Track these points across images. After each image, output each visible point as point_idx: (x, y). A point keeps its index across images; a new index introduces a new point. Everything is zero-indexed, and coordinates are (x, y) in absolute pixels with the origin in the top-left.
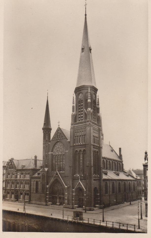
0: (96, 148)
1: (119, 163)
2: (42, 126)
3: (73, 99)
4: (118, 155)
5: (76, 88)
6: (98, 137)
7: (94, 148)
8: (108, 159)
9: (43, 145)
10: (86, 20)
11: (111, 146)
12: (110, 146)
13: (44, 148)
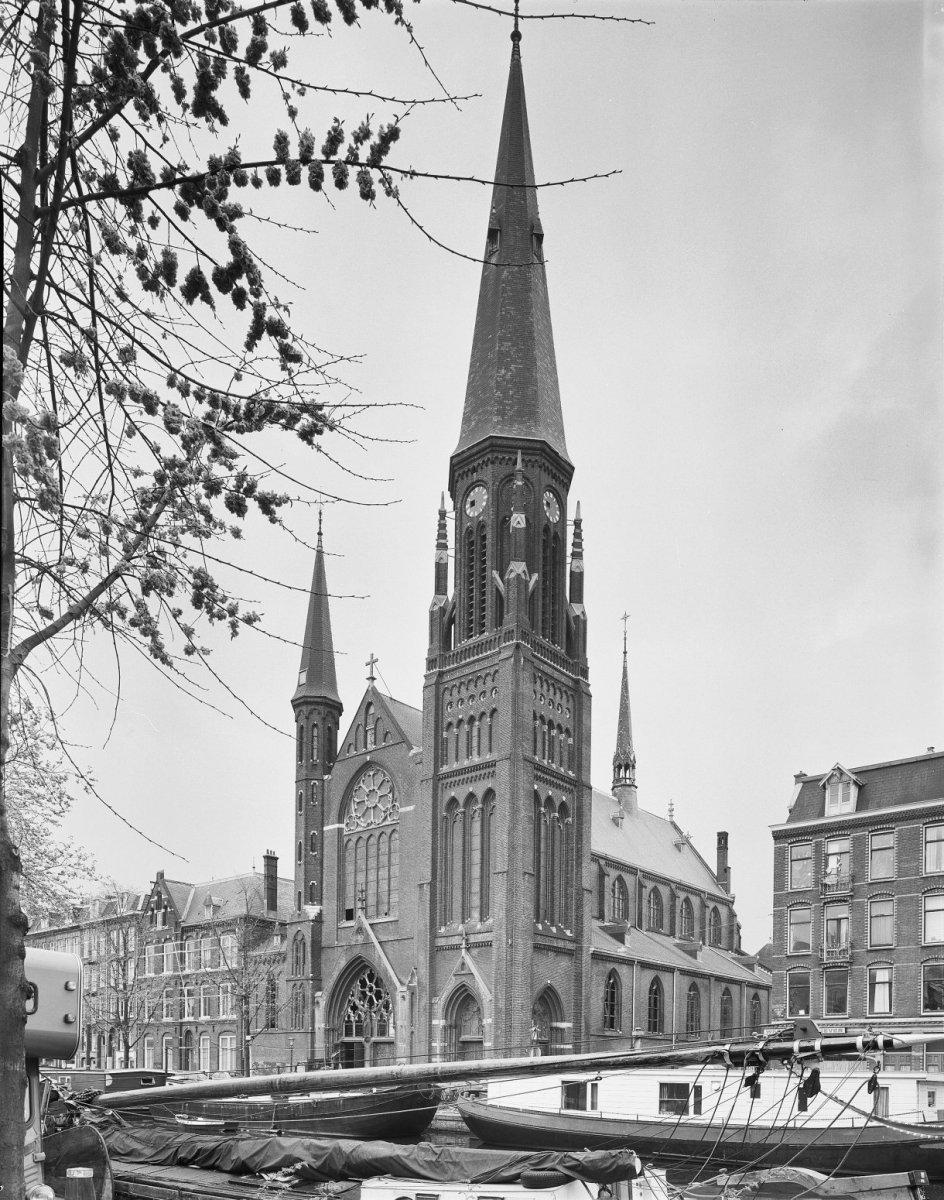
0: (558, 787)
1: (711, 905)
3: (442, 526)
4: (713, 874)
5: (452, 458)
6: (567, 731)
8: (644, 877)
9: (297, 789)
11: (676, 827)
12: (673, 823)
13: (300, 803)
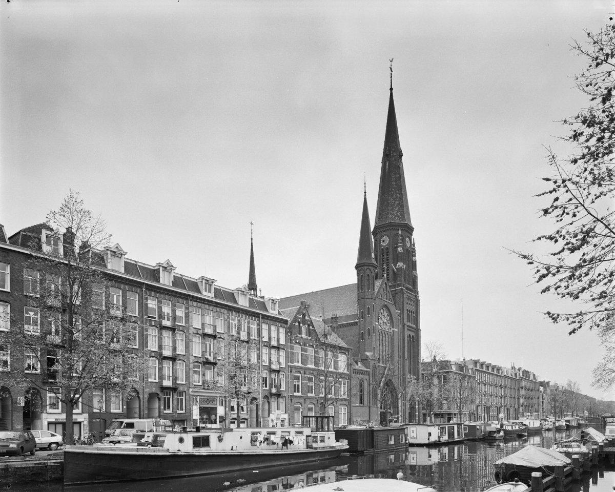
7: (408, 329)
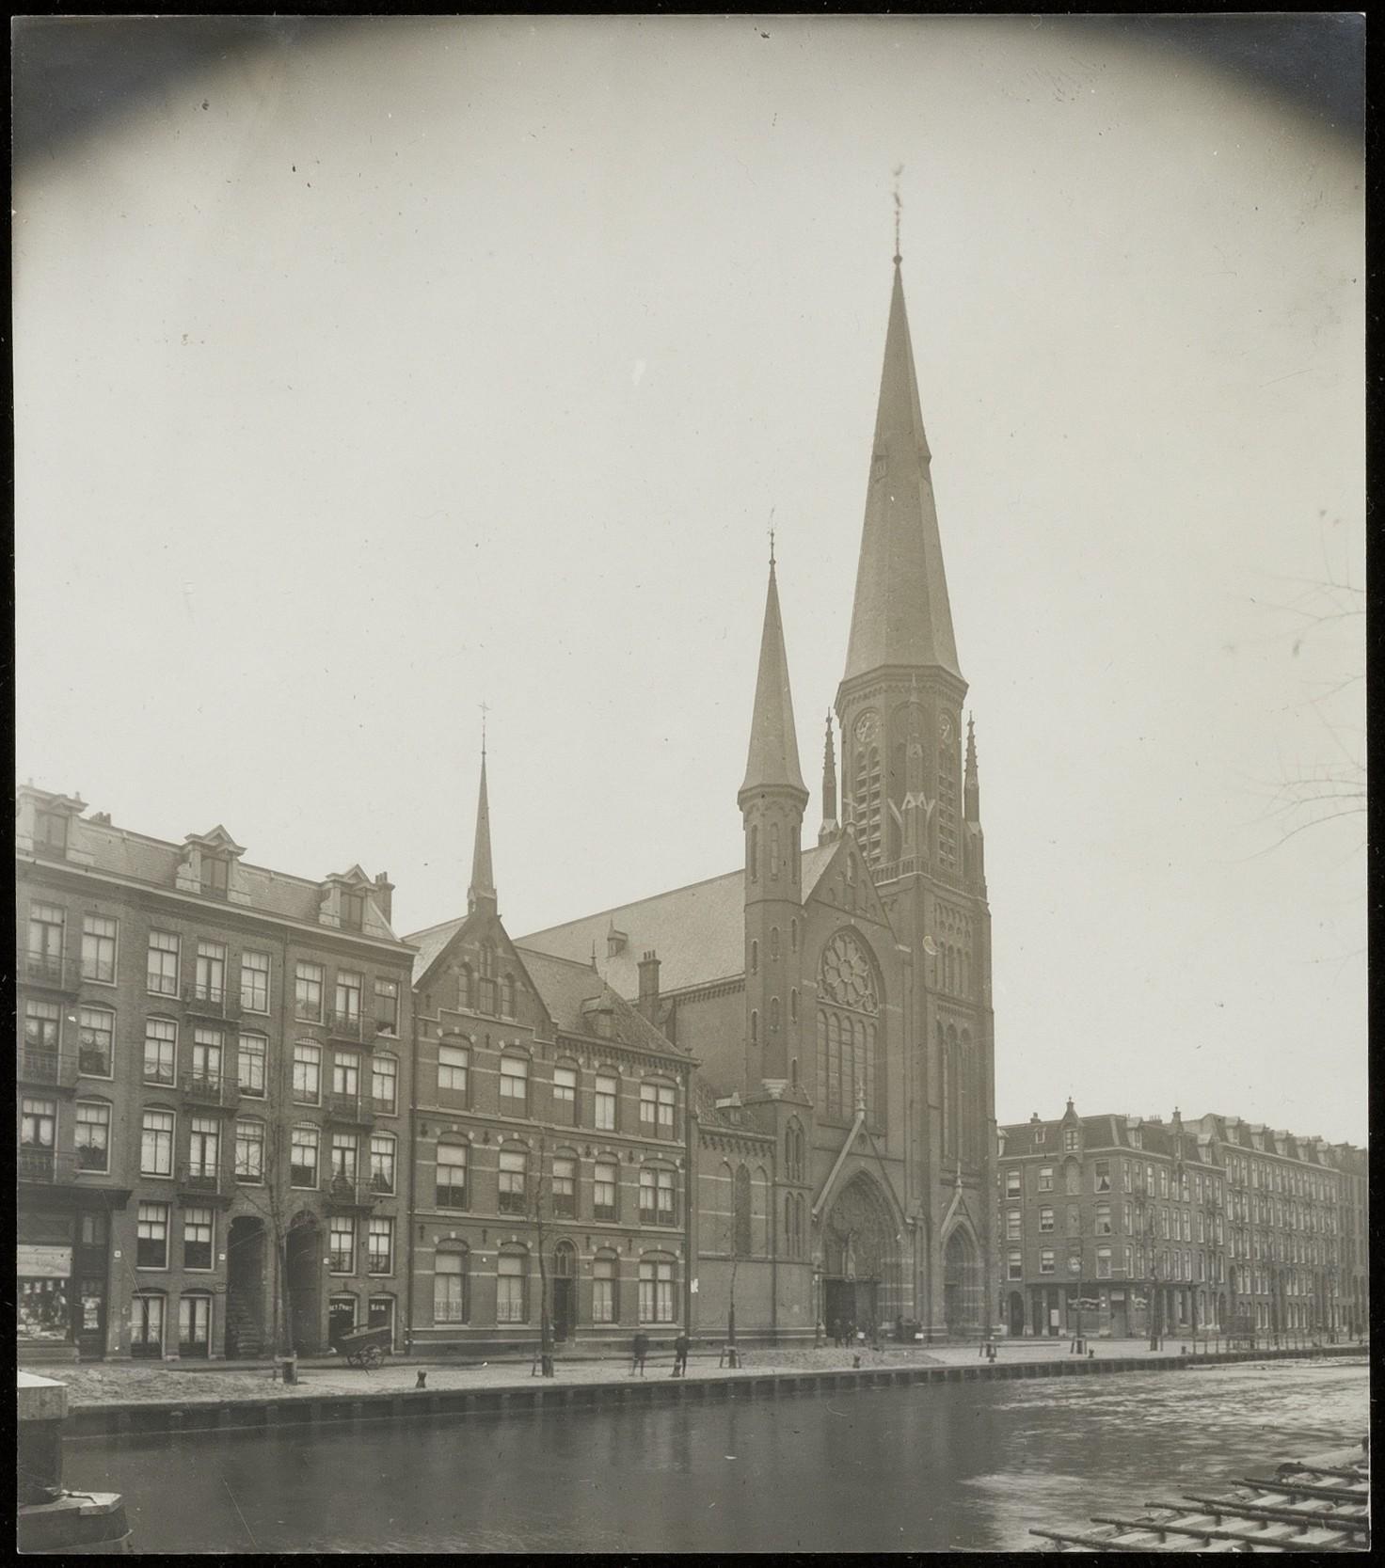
2: (734, 771)
3: (829, 745)
10: (775, 585)
